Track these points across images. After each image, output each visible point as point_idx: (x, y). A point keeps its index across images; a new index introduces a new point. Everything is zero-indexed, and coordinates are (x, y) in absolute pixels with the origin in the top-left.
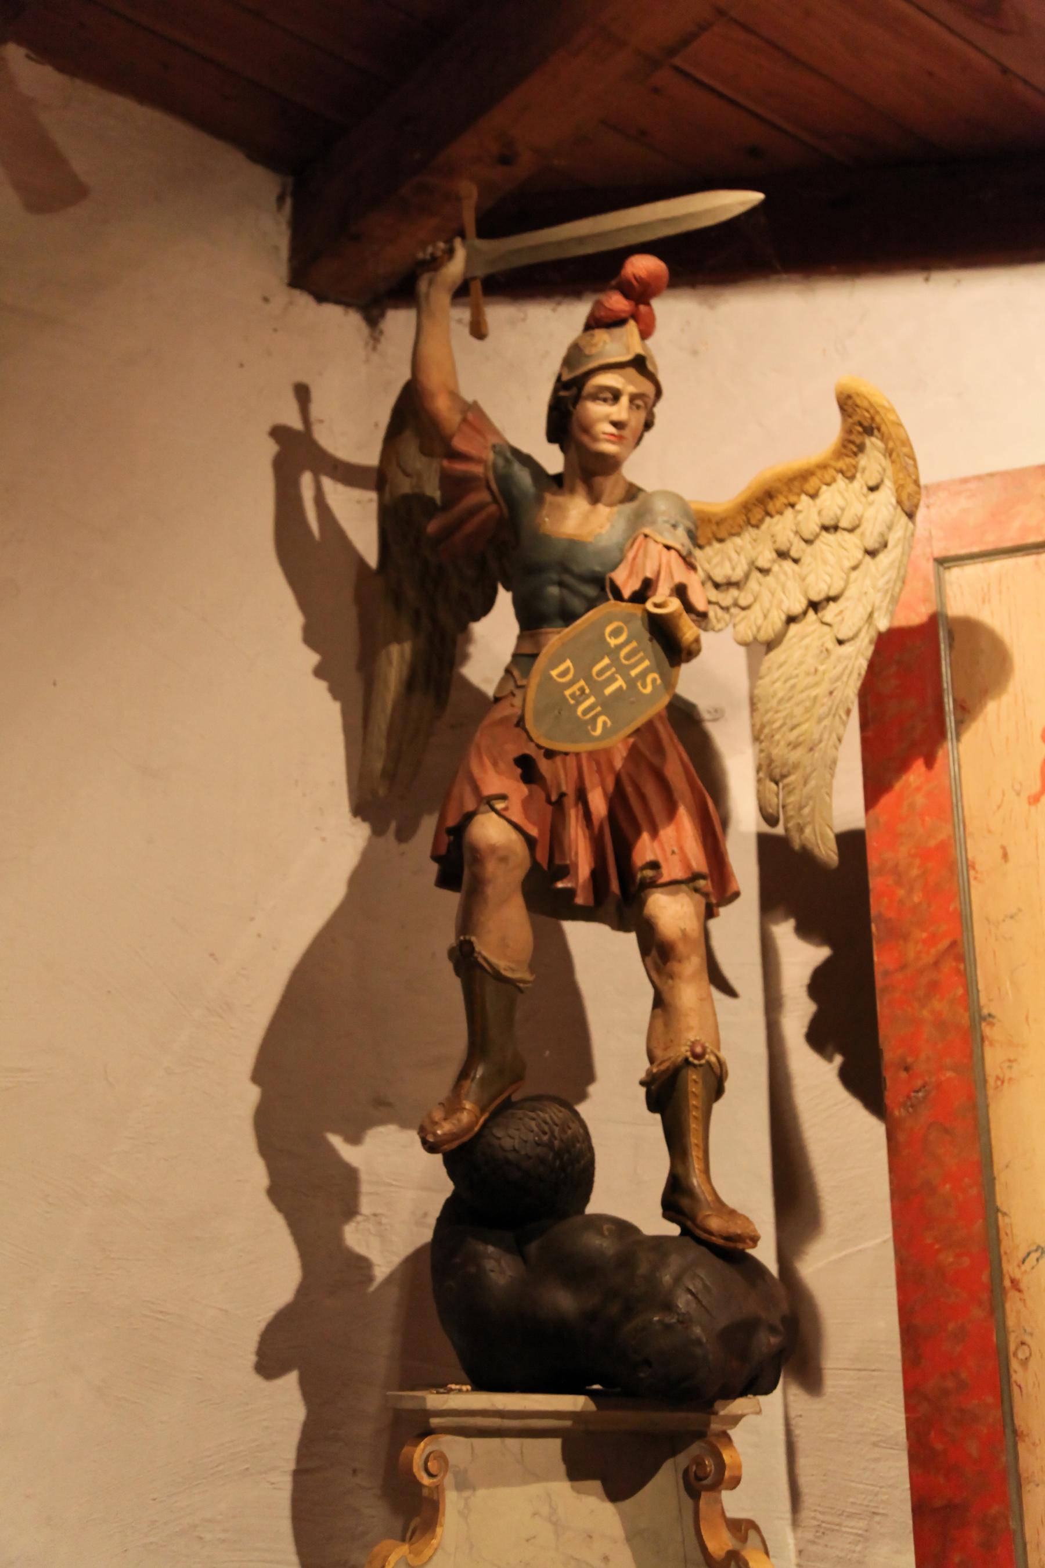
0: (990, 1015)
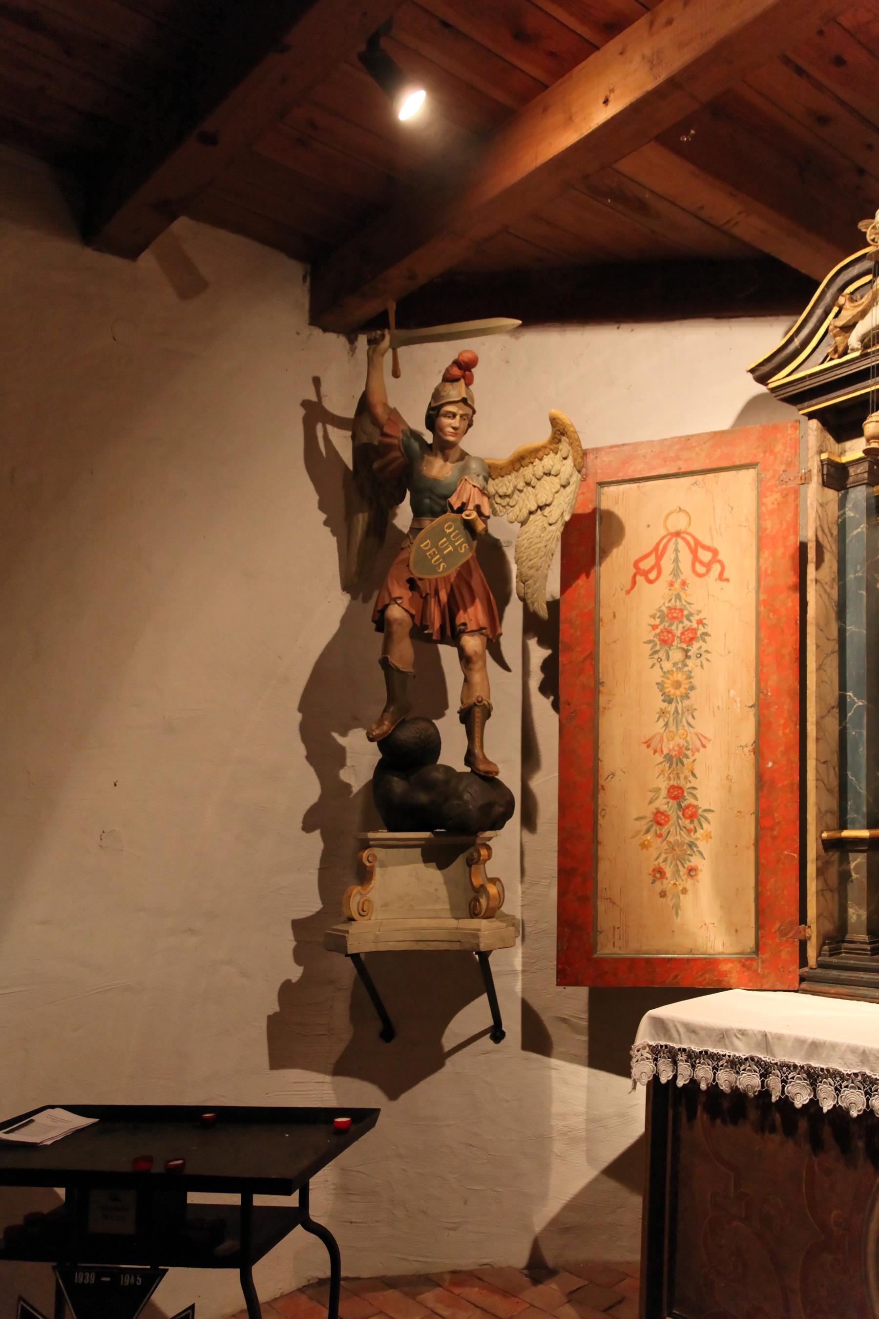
0: (603, 682)
